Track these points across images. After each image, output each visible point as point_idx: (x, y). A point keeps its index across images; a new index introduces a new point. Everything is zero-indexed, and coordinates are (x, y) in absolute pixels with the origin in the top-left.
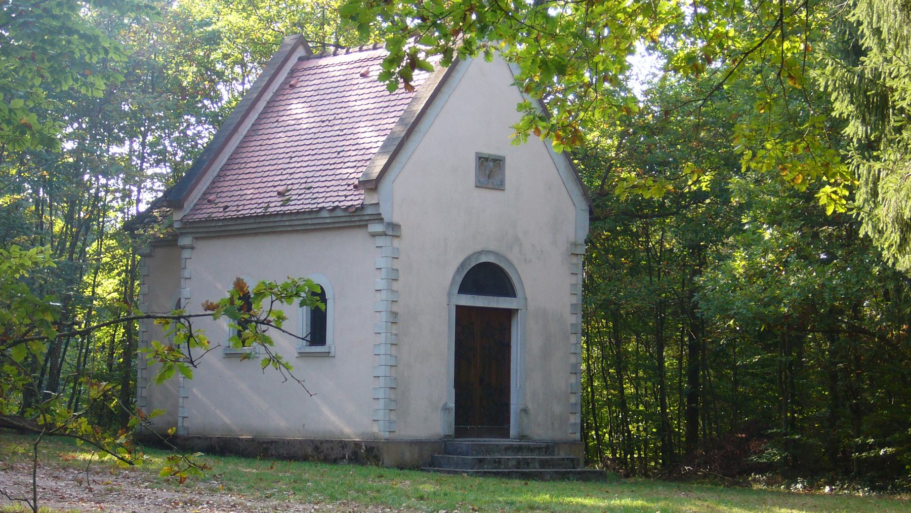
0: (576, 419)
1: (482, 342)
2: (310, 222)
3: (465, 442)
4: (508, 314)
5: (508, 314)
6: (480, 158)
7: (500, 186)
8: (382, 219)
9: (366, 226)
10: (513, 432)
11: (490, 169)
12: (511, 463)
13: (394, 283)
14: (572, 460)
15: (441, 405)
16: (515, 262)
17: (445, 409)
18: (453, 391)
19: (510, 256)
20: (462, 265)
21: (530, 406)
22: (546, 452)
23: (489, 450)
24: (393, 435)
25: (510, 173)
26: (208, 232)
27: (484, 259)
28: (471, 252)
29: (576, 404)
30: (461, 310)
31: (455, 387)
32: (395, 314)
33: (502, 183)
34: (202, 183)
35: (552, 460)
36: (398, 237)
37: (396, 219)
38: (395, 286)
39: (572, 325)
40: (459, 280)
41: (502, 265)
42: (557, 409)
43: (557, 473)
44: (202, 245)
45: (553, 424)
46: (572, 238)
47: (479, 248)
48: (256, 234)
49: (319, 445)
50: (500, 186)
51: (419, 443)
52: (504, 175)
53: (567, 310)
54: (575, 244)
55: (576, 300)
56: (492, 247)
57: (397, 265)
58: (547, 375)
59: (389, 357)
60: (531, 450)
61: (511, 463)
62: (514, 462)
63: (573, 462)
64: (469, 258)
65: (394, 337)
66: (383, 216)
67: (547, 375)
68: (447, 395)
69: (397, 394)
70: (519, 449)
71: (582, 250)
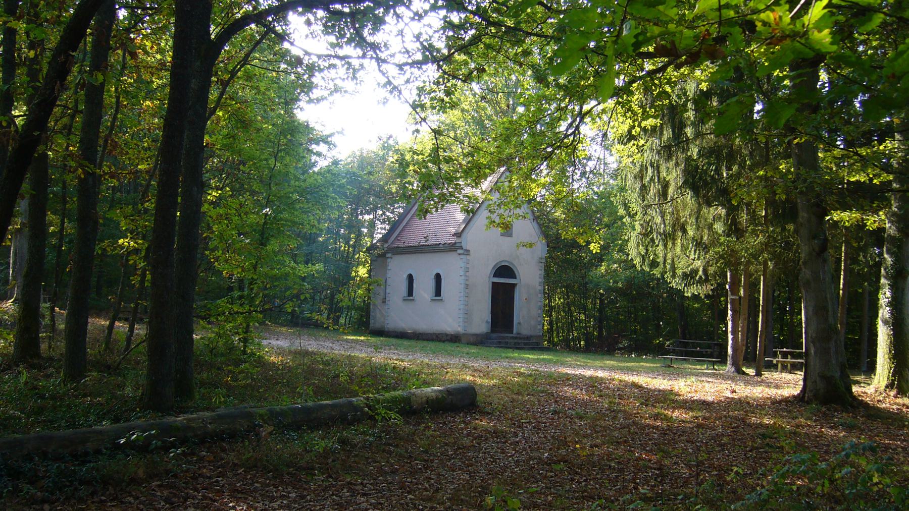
1: (503, 295)
4: (513, 286)
5: (513, 286)
7: (510, 235)
17: (487, 322)
23: (504, 338)
42: (533, 323)
50: (510, 235)
51: (476, 335)
53: (538, 284)
56: (507, 259)
60: (520, 338)
67: (528, 312)
69: (468, 315)
70: (516, 338)
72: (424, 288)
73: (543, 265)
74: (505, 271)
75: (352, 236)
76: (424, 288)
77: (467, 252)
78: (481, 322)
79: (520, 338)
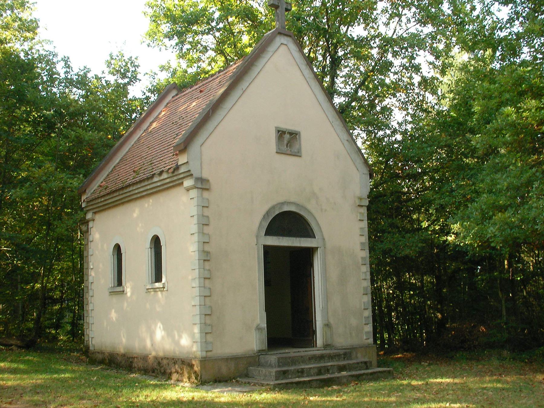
0: (369, 328)
1: (288, 274)
2: (148, 187)
3: (273, 358)
4: (309, 252)
5: (309, 252)
6: (279, 131)
7: (297, 154)
8: (192, 175)
9: (182, 183)
10: (319, 342)
11: (288, 140)
12: (312, 372)
13: (205, 227)
14: (366, 363)
15: (255, 326)
16: (313, 211)
17: (258, 329)
18: (264, 314)
19: (309, 207)
20: (268, 213)
21: (332, 321)
22: (344, 358)
23: (294, 361)
24: (209, 354)
25: (306, 142)
26: (98, 207)
27: (286, 208)
28: (274, 203)
29: (368, 317)
30: (268, 251)
31: (267, 310)
32: (208, 253)
33: (299, 151)
34: (100, 176)
35: (349, 364)
36: (207, 189)
37: (205, 175)
38: (206, 229)
39: (362, 258)
40: (266, 225)
41: (302, 213)
42: (354, 322)
43: (352, 376)
44: (97, 217)
45: (351, 334)
46: (358, 193)
47: (281, 200)
48: (123, 203)
49: (160, 361)
50: (297, 154)
51: (235, 359)
52: (300, 145)
53: (358, 247)
54: (361, 199)
55: (365, 239)
56: (292, 200)
57: (207, 212)
58: (343, 298)
59: (203, 289)
60: (331, 357)
61: (312, 372)
62: (316, 370)
63: (366, 365)
64: (273, 207)
65: (206, 272)
66: (192, 172)
67: (343, 298)
68: (258, 316)
69: (210, 319)
70: (321, 357)
71: (366, 202)
72: (138, 262)
73: (364, 211)
74: (289, 222)
75: (430, 233)
76: (138, 262)
77: (203, 184)
78: (247, 324)
79: (331, 357)
